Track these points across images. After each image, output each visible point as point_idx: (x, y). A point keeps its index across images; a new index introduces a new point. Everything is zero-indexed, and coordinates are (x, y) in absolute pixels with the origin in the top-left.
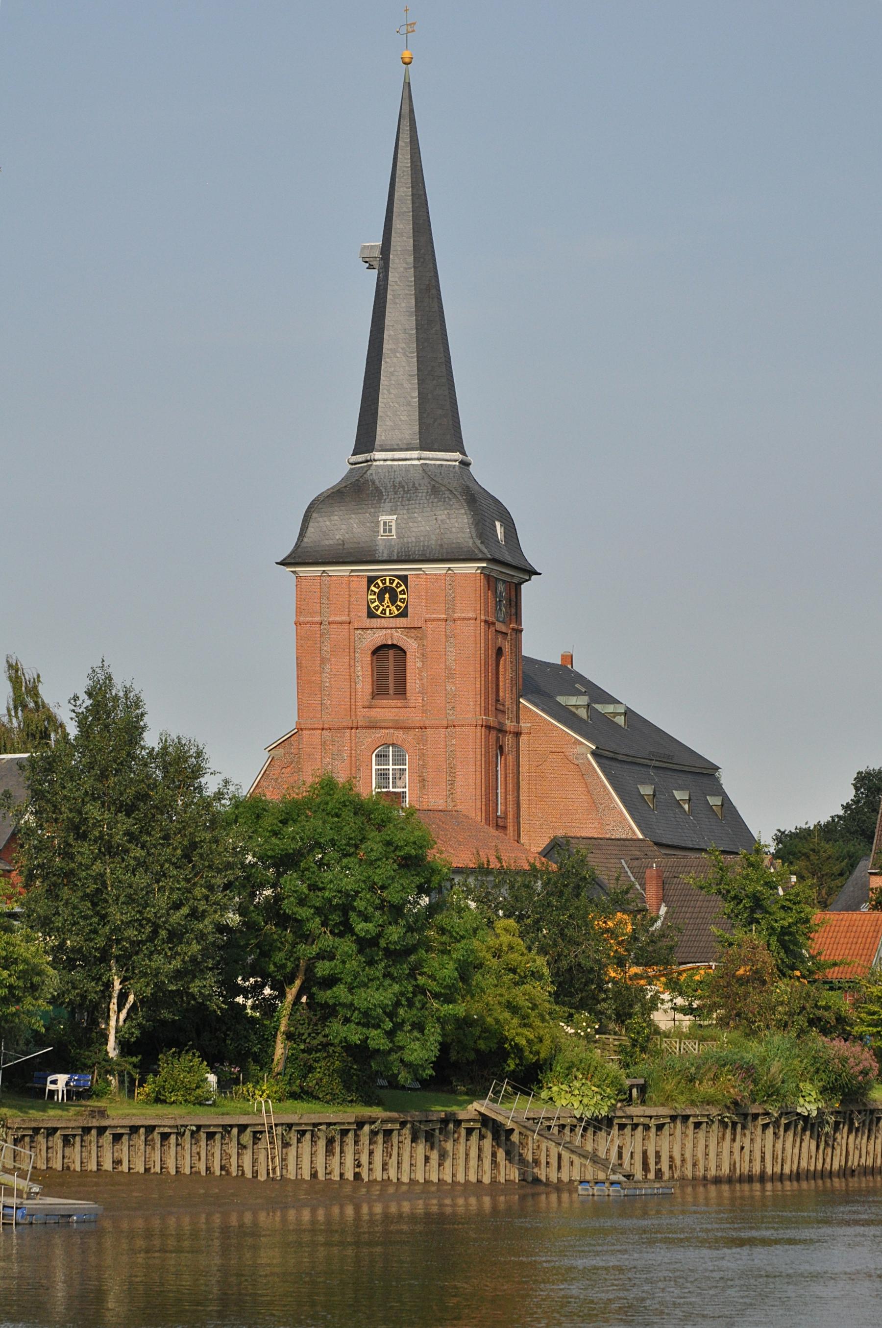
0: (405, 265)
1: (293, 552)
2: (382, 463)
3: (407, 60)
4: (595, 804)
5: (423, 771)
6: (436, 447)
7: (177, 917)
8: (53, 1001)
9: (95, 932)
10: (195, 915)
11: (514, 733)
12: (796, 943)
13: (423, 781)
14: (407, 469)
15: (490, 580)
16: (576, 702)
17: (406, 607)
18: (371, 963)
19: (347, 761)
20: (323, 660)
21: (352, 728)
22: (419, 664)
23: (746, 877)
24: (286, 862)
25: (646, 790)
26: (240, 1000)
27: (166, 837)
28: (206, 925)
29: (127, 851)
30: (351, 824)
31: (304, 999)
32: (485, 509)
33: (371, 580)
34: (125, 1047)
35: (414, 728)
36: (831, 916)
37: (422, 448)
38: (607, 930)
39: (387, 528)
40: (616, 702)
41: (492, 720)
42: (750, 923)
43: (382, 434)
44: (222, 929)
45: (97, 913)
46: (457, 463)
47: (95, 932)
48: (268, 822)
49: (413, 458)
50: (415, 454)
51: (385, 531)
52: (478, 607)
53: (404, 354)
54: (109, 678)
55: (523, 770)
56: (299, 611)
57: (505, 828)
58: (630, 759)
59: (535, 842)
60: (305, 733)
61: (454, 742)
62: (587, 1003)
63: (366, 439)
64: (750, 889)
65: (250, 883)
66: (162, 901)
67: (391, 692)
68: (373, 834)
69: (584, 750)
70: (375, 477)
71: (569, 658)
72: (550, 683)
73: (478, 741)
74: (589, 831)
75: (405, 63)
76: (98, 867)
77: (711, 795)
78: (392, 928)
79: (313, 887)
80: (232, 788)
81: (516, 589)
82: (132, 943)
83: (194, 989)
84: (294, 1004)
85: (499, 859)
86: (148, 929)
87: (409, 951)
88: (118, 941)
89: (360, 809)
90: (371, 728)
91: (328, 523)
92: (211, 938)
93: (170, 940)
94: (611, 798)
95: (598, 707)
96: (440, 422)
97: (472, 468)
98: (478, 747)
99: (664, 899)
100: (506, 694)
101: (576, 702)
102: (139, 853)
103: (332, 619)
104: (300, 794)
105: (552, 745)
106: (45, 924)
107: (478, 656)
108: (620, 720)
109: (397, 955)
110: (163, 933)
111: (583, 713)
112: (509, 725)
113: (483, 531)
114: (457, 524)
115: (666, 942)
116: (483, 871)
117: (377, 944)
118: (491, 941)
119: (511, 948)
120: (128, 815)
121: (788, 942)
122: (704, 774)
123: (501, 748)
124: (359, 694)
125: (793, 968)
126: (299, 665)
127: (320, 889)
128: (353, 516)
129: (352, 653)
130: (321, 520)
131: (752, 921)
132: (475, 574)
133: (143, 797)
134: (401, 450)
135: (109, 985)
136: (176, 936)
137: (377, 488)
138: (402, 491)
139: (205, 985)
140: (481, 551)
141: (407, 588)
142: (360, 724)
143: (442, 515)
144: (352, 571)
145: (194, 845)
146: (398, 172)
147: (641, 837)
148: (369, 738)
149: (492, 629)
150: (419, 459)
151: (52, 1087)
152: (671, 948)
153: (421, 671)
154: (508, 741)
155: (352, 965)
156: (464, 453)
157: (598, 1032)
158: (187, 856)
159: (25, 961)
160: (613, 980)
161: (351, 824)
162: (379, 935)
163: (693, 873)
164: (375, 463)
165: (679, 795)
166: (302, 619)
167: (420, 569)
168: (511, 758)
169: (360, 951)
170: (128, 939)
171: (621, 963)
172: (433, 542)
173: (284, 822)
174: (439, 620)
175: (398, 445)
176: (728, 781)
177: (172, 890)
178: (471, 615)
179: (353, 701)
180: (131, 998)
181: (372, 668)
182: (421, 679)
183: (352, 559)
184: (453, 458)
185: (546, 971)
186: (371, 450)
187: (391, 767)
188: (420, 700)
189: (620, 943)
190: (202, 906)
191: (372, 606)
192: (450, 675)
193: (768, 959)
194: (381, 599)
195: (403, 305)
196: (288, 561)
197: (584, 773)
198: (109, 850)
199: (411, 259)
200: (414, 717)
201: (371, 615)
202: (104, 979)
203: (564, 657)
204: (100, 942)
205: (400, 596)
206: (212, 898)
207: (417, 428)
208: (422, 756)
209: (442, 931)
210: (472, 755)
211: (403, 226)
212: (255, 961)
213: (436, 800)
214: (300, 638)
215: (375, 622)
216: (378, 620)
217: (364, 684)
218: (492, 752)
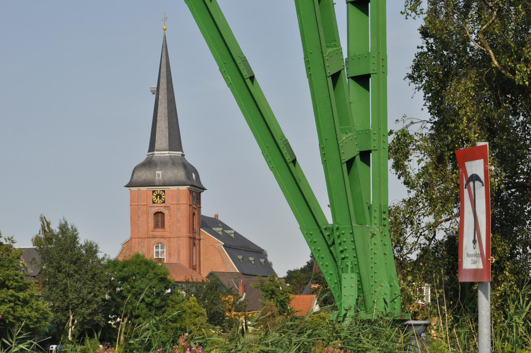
4: (224, 261)
5: (169, 252)
7: (90, 296)
8: (52, 322)
9: (64, 301)
10: (95, 296)
12: (285, 305)
15: (191, 192)
16: (218, 230)
18: (150, 311)
20: (139, 217)
22: (169, 218)
23: (269, 285)
24: (124, 279)
25: (240, 257)
26: (110, 322)
27: (86, 272)
28: (99, 299)
29: (74, 276)
30: (144, 268)
31: (130, 322)
32: (189, 169)
34: (73, 336)
36: (297, 296)
37: (170, 150)
38: (226, 301)
39: (159, 176)
40: (230, 229)
41: (191, 235)
42: (271, 298)
43: (157, 146)
44: (104, 300)
45: (65, 295)
47: (64, 301)
48: (119, 267)
49: (167, 153)
50: (167, 152)
54: (66, 222)
56: (131, 201)
57: (196, 269)
59: (205, 274)
60: (133, 240)
62: (219, 323)
63: (152, 148)
64: (271, 288)
65: (112, 286)
66: (85, 291)
68: (151, 271)
71: (217, 216)
72: (210, 224)
74: (222, 270)
76: (65, 281)
77: (261, 259)
78: (156, 300)
79: (132, 287)
80: (107, 257)
81: (199, 194)
82: (76, 304)
83: (95, 319)
84: (127, 323)
85: (192, 278)
86: (81, 300)
87: (162, 307)
88: (71, 304)
89: (147, 263)
92: (100, 303)
93: (87, 303)
94: (229, 260)
95: (226, 231)
96: (175, 143)
97: (185, 157)
99: (245, 291)
100: (196, 227)
101: (218, 230)
102: (77, 276)
104: (128, 259)
106: (47, 298)
108: (233, 235)
109: (159, 308)
110: (85, 301)
111: (220, 233)
112: (197, 237)
113: (189, 176)
114: (180, 174)
115: (244, 304)
116: (187, 282)
117: (152, 305)
118: (188, 304)
119: (194, 306)
120: (74, 265)
121: (283, 304)
122: (260, 253)
123: (194, 244)
125: (284, 312)
126: (131, 218)
127: (135, 288)
131: (271, 298)
133: (79, 259)
135: (69, 317)
136: (89, 302)
137: (155, 163)
138: (163, 163)
139: (99, 318)
143: (176, 171)
145: (95, 274)
147: (238, 271)
148: (153, 241)
151: (51, 349)
152: (245, 306)
154: (197, 242)
155: (144, 311)
156: (183, 152)
157: (222, 332)
158: (93, 278)
159: (43, 310)
160: (227, 316)
161: (144, 268)
162: (153, 302)
163: (253, 283)
165: (251, 259)
168: (198, 247)
169: (147, 307)
170: (74, 303)
171: (230, 311)
173: (123, 267)
177: (88, 288)
178: (185, 202)
180: (76, 322)
185: (205, 313)
186: (153, 151)
187: (160, 250)
189: (230, 305)
190: (97, 293)
192: (178, 221)
193: (276, 310)
194: (157, 197)
197: (221, 252)
198: (69, 276)
199: (166, 91)
200: (167, 234)
202: (67, 315)
204: (66, 304)
206: (101, 291)
207: (168, 144)
208: (170, 247)
209: (172, 301)
211: (163, 81)
212: (115, 310)
213: (174, 260)
215: (155, 205)
217: (151, 224)
218: (192, 245)
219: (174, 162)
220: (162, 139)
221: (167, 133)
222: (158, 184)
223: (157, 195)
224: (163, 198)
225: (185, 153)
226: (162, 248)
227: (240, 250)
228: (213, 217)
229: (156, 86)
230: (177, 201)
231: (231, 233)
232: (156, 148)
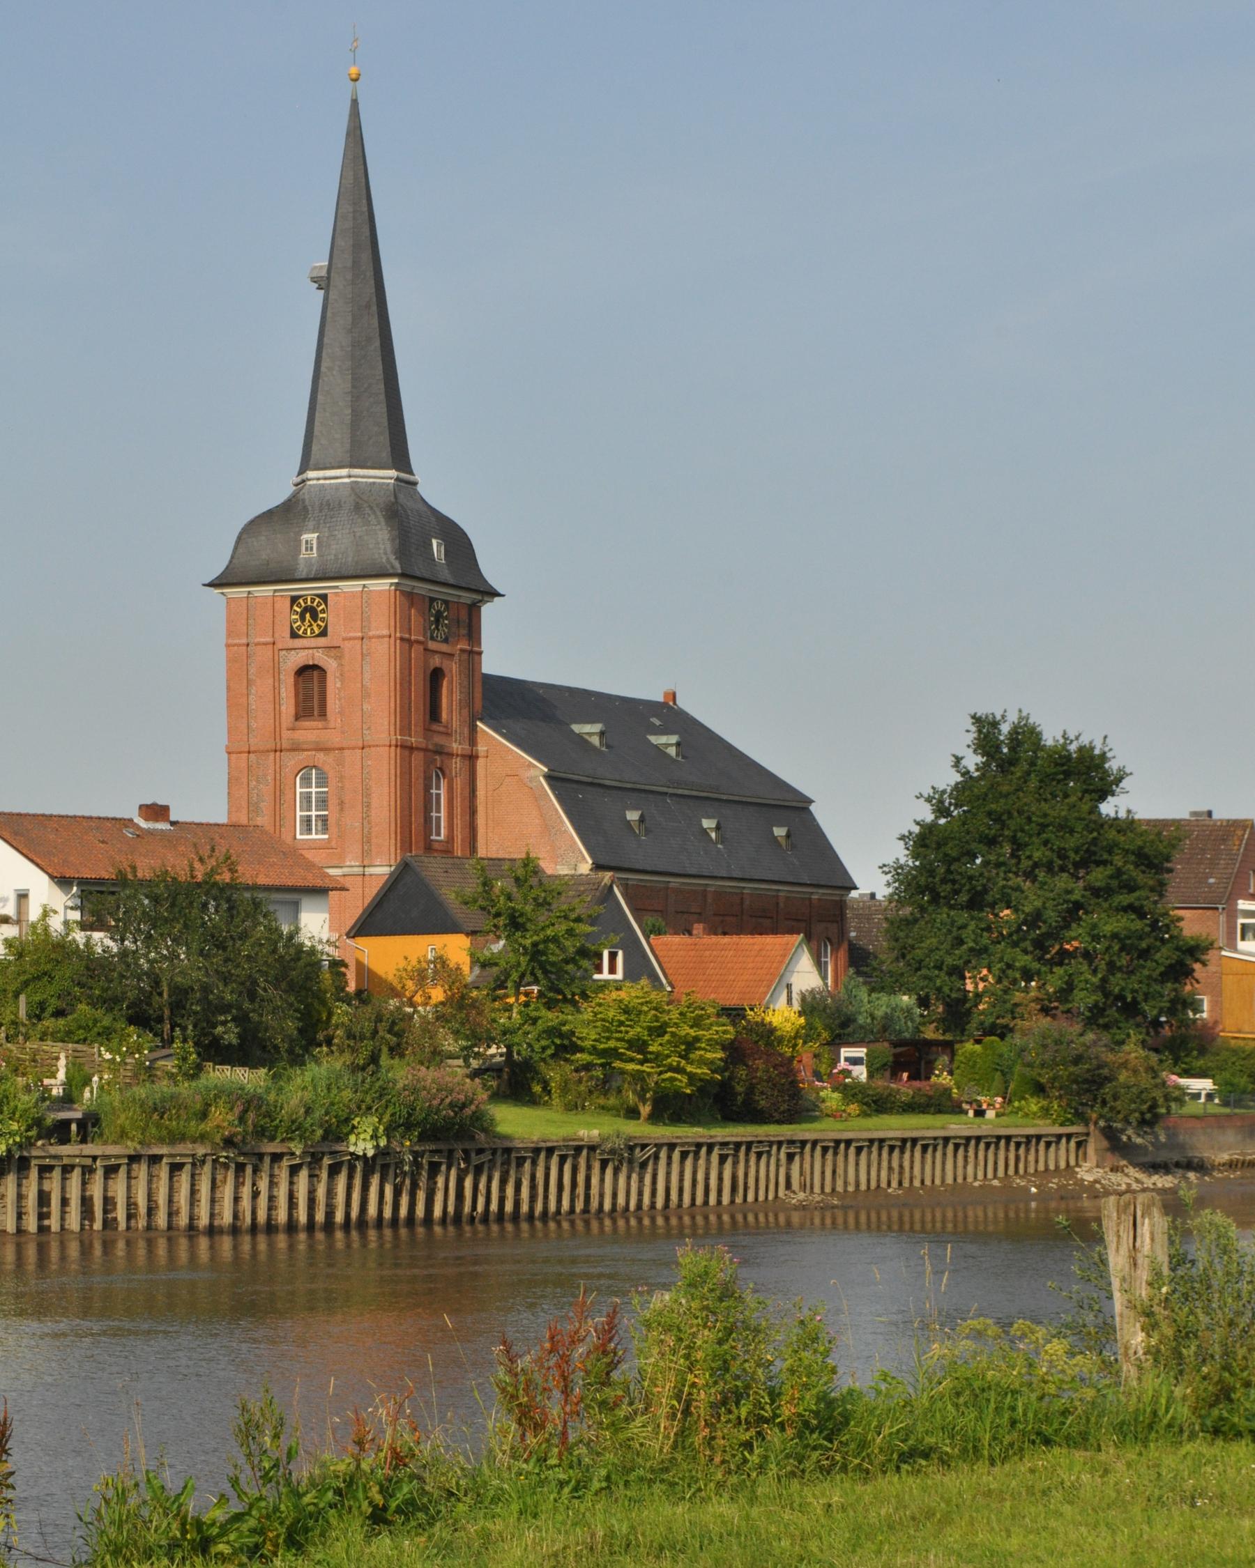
3: (354, 76)
11: (463, 756)
14: (337, 487)
33: (294, 600)
35: (334, 749)
37: (352, 466)
50: (344, 472)
55: (481, 793)
56: (230, 634)
58: (629, 786)
69: (537, 773)
70: (307, 497)
72: (528, 709)
75: (353, 80)
90: (294, 750)
97: (419, 488)
103: (257, 640)
122: (796, 808)
124: (283, 716)
126: (228, 688)
134: (333, 468)
137: (305, 508)
140: (393, 567)
144: (275, 591)
148: (292, 761)
150: (350, 476)
165: (708, 824)
166: (230, 641)
167: (337, 587)
168: (458, 783)
172: (350, 559)
176: (820, 812)
178: (385, 632)
183: (273, 578)
187: (314, 790)
191: (295, 626)
194: (303, 619)
197: (538, 797)
200: (334, 738)
201: (294, 635)
203: (666, 695)
207: (348, 446)
208: (341, 779)
210: (386, 777)
217: (288, 707)
223: (306, 610)
224: (323, 620)
228: (661, 699)
231: (590, 734)
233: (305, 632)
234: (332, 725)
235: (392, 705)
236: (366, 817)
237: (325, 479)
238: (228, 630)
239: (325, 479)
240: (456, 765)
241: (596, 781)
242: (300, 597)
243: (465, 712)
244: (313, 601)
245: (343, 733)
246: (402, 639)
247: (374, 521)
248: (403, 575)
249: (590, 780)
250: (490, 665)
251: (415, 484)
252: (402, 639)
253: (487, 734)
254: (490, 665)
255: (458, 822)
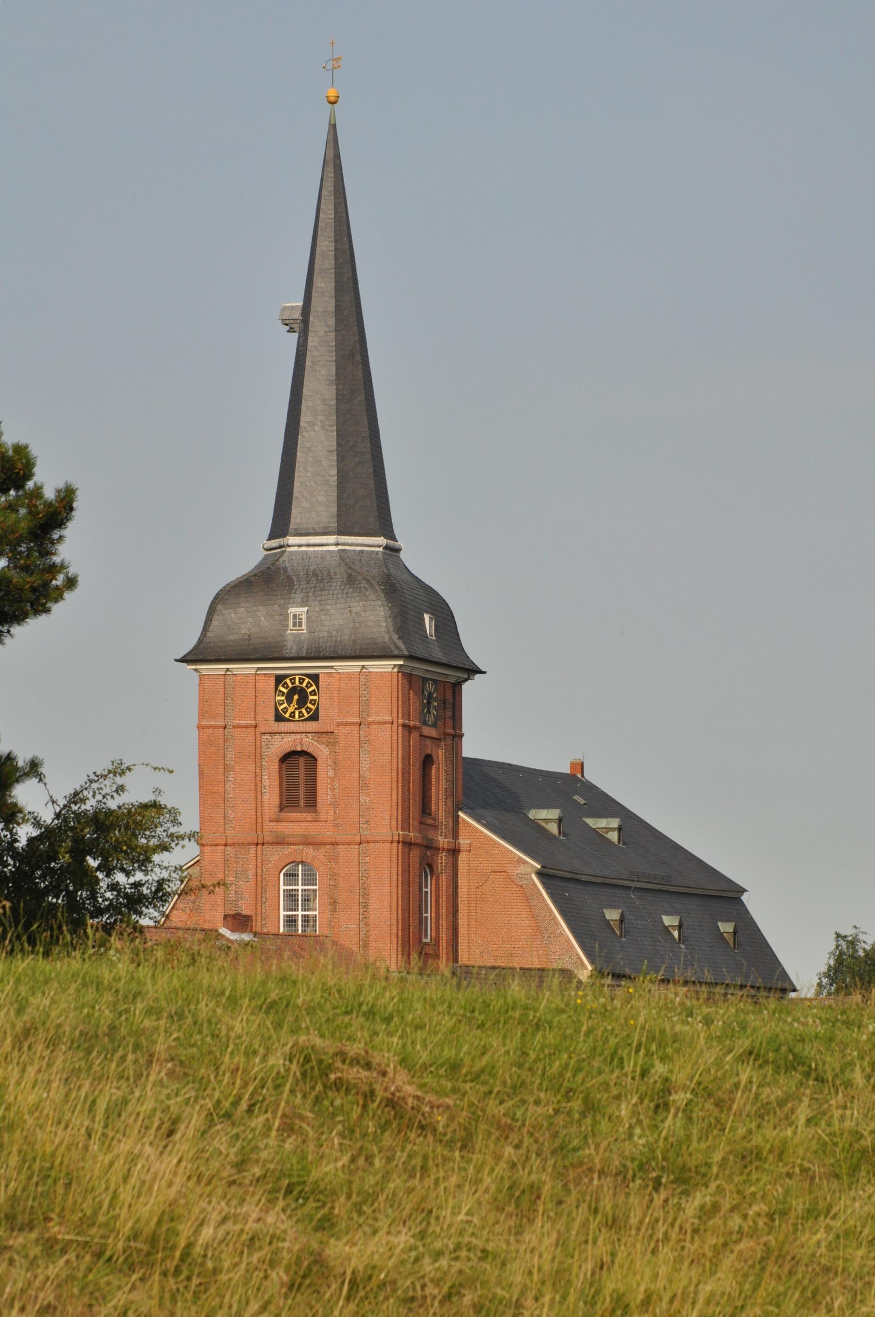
0: (326, 329)
1: (196, 647)
2: (296, 549)
3: (332, 99)
6: (356, 530)
11: (448, 850)
13: (334, 903)
15: (409, 677)
17: (317, 709)
19: (252, 881)
20: (226, 769)
21: (257, 844)
22: (331, 773)
35: (325, 844)
37: (340, 533)
39: (297, 622)
43: (297, 517)
46: (381, 549)
49: (329, 543)
50: (332, 539)
51: (294, 625)
52: (395, 709)
53: (323, 427)
56: (202, 714)
58: (600, 880)
61: (367, 860)
63: (281, 525)
67: (302, 803)
70: (288, 565)
72: (499, 792)
73: (394, 859)
75: (331, 103)
77: (722, 921)
90: (278, 843)
91: (233, 616)
94: (557, 924)
96: (365, 501)
97: (402, 555)
98: (394, 865)
103: (236, 722)
105: (494, 864)
107: (394, 765)
112: (443, 841)
114: (374, 617)
122: (726, 897)
124: (266, 806)
126: (201, 774)
128: (261, 608)
129: (258, 761)
130: (226, 612)
132: (392, 673)
137: (289, 578)
138: (316, 579)
140: (397, 647)
141: (318, 687)
142: (267, 839)
144: (259, 669)
146: (321, 225)
148: (276, 856)
149: (415, 735)
150: (337, 544)
153: (332, 781)
164: (289, 549)
166: (204, 723)
167: (332, 667)
168: (444, 879)
172: (346, 637)
174: (351, 724)
175: (314, 529)
178: (387, 718)
179: (259, 814)
181: (280, 778)
182: (333, 790)
183: (258, 656)
184: (375, 543)
186: (284, 535)
188: (331, 812)
191: (280, 708)
195: (323, 372)
196: (189, 658)
199: (332, 322)
200: (326, 832)
201: (279, 718)
203: (573, 765)
205: (311, 697)
207: (334, 510)
208: (334, 876)
210: (386, 874)
211: (325, 285)
214: (202, 743)
216: (287, 724)
217: (271, 796)
219: (352, 574)
220: (316, 494)
221: (334, 472)
222: (294, 653)
223: (293, 690)
224: (313, 702)
225: (400, 543)
226: (309, 879)
227: (629, 888)
228: (567, 770)
229: (301, 304)
230: (360, 713)
231: (546, 821)
232: (292, 526)
233: (293, 714)
234: (323, 816)
235: (394, 797)
236: (364, 917)
237: (308, 545)
238: (200, 710)
239: (308, 545)
240: (442, 860)
241: (576, 876)
242: (286, 676)
243: (450, 801)
244: (301, 681)
245: (335, 826)
246: (404, 726)
247: (373, 597)
248: (411, 657)
249: (570, 876)
250: (470, 749)
251: (398, 550)
252: (404, 726)
253: (470, 825)
254: (470, 749)
255: (443, 922)
